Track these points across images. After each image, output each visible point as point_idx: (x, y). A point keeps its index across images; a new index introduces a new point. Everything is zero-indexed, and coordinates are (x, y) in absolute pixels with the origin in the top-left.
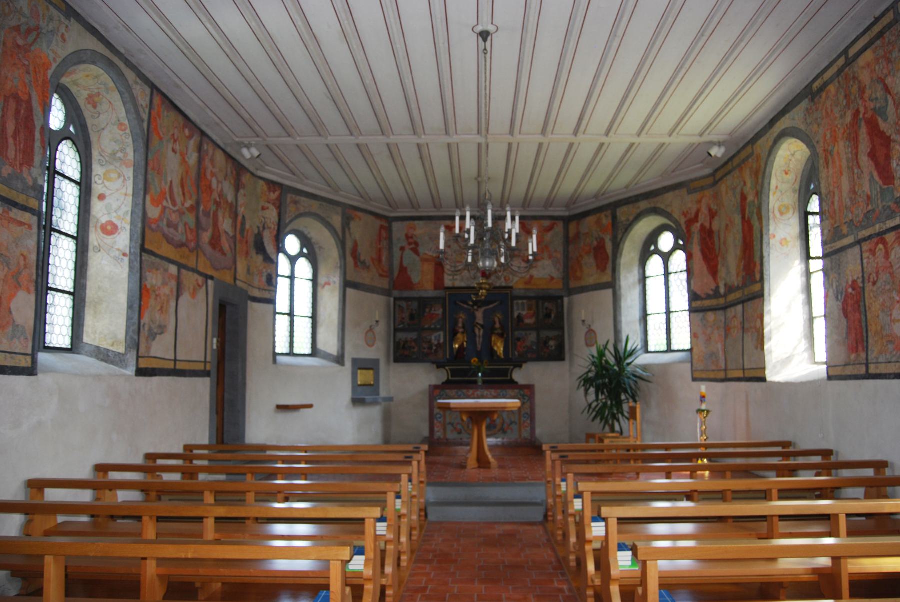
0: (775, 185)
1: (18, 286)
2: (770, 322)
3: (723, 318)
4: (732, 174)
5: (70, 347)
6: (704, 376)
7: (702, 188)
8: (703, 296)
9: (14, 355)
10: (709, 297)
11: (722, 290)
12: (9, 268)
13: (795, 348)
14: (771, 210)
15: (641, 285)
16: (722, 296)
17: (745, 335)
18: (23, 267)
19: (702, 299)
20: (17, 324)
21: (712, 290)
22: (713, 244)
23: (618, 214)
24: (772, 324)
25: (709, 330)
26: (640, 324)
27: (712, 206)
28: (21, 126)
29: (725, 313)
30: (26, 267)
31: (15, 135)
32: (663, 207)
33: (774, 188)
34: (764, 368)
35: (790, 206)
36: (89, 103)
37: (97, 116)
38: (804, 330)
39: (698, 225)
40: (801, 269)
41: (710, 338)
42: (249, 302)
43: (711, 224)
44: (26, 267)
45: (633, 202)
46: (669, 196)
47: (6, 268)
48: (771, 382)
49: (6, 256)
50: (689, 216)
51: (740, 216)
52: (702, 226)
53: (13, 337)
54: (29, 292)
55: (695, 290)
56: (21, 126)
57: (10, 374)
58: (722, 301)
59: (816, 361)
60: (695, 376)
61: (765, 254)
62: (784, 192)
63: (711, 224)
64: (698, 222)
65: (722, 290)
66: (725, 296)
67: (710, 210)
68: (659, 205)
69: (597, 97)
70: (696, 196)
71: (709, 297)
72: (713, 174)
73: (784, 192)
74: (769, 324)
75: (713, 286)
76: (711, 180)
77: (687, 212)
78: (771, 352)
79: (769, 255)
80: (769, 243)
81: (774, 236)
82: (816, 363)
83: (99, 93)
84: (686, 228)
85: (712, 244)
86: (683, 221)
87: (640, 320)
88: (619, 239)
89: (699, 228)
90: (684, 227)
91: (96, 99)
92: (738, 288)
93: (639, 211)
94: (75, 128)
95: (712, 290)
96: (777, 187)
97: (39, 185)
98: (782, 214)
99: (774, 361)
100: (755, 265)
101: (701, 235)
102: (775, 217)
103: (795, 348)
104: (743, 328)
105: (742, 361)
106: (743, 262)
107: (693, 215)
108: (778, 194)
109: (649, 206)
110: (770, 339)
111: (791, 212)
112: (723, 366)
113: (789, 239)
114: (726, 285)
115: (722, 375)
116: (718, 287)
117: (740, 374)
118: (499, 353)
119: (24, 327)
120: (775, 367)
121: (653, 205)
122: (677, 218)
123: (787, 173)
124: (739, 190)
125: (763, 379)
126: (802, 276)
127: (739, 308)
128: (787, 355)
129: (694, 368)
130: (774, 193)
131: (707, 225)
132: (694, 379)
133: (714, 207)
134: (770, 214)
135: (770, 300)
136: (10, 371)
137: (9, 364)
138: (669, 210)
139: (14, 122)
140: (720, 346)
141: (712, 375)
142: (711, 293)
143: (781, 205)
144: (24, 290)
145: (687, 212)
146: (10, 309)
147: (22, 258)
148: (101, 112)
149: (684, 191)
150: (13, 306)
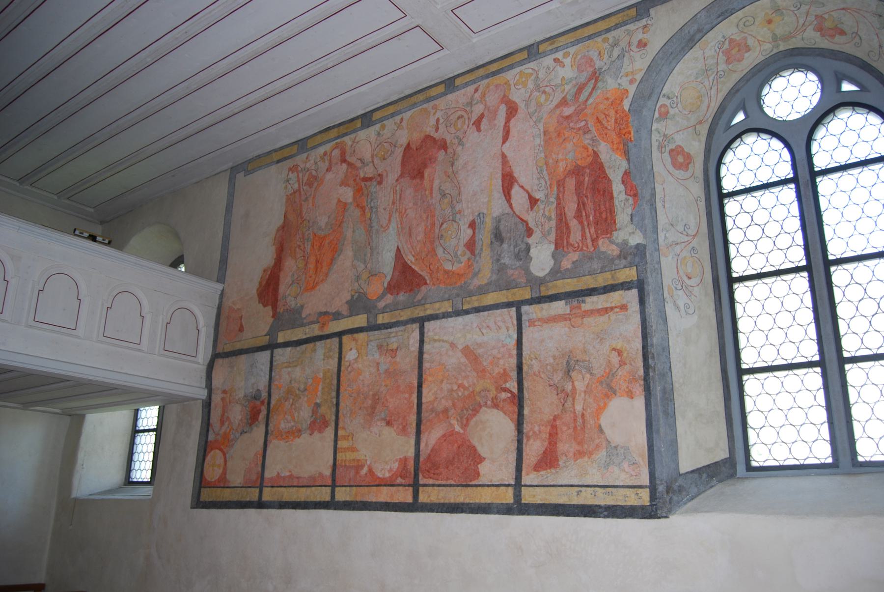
1: (611, 392)
5: (830, 460)
9: (614, 490)
12: (591, 374)
18: (617, 366)
20: (613, 445)
28: (586, 197)
30: (622, 363)
31: (578, 216)
36: (833, 36)
37: (857, 40)
42: (158, 407)
44: (622, 363)
47: (588, 376)
49: (584, 361)
53: (607, 466)
54: (631, 395)
56: (586, 197)
57: (605, 517)
69: (12, 28)
83: (817, 17)
91: (828, 24)
94: (852, 81)
97: (631, 247)
119: (627, 449)
136: (606, 513)
137: (602, 503)
139: (575, 199)
144: (622, 396)
146: (600, 426)
147: (615, 354)
148: (855, 30)
150: (604, 421)
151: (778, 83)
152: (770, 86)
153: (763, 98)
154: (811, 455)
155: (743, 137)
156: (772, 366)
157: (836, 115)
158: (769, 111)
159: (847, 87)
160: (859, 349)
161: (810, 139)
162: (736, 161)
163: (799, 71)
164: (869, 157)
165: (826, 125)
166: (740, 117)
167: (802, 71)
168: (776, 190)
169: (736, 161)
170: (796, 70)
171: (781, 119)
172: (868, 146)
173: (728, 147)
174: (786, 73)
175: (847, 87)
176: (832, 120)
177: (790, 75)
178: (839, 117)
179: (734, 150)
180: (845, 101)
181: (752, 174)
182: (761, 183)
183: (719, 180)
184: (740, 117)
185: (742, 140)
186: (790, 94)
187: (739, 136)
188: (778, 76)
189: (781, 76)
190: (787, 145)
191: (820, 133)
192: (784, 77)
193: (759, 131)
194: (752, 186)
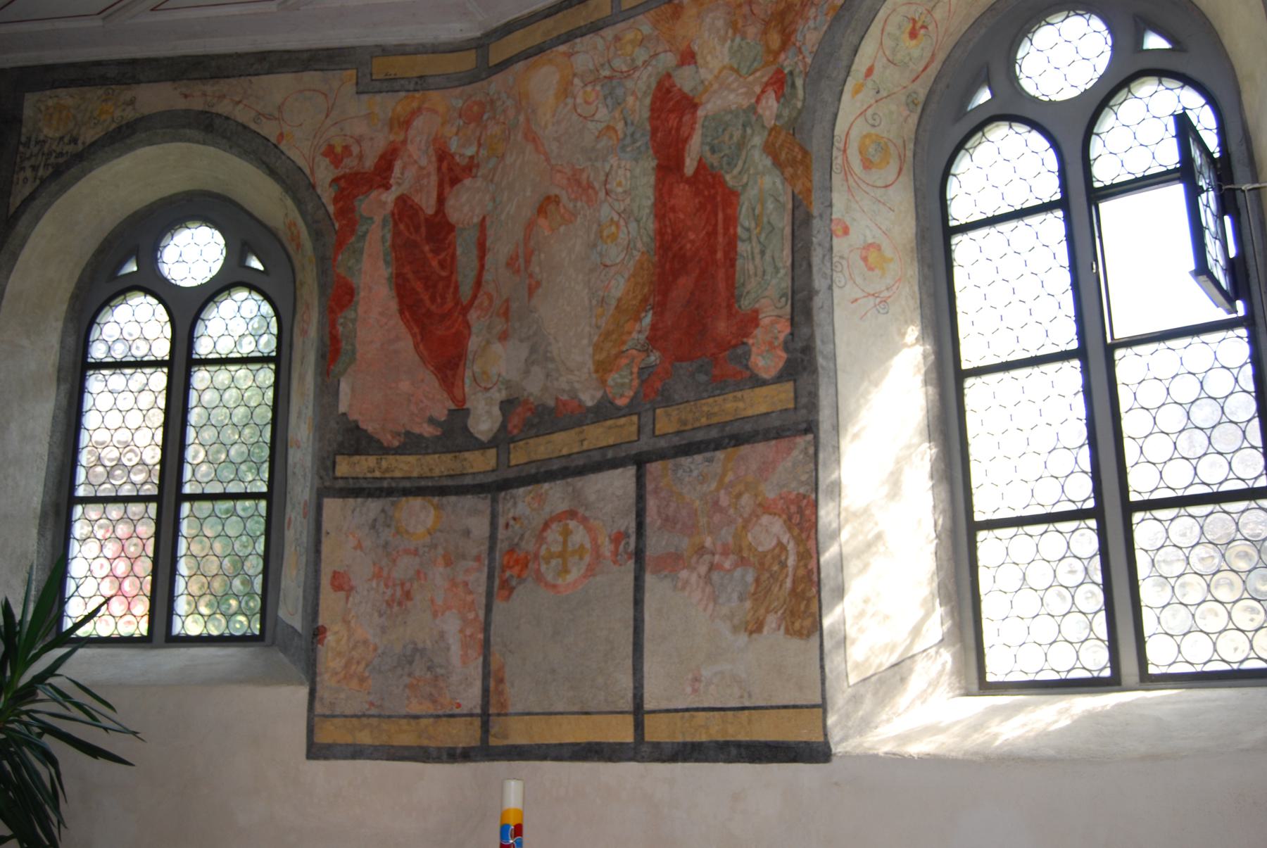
0: (868, 64)
2: (839, 529)
3: (480, 527)
4: (609, 33)
5: (1107, 673)
6: (365, 738)
7: (422, 83)
8: (387, 439)
10: (412, 444)
11: (484, 422)
13: (916, 631)
14: (838, 144)
15: (65, 387)
16: (482, 446)
17: (649, 579)
19: (384, 450)
21: (432, 421)
22: (450, 264)
23: (28, 112)
24: (845, 535)
25: (405, 567)
26: (41, 534)
27: (454, 146)
29: (494, 501)
32: (242, 115)
33: (864, 70)
34: (822, 707)
35: (892, 149)
38: (939, 568)
39: (389, 197)
40: (925, 357)
41: (408, 595)
43: (441, 200)
45: (104, 81)
46: (279, 86)
48: (846, 756)
50: (350, 164)
51: (650, 163)
52: (402, 200)
55: (354, 416)
58: (480, 463)
59: (990, 678)
60: (322, 738)
61: (819, 283)
62: (884, 93)
63: (441, 200)
64: (387, 187)
65: (484, 422)
66: (501, 440)
67: (443, 156)
68: (223, 108)
70: (387, 105)
71: (412, 444)
72: (480, 45)
73: (884, 93)
74: (836, 534)
75: (440, 408)
76: (468, 61)
77: (346, 148)
78: (843, 642)
79: (830, 288)
80: (831, 248)
81: (846, 231)
82: (987, 688)
84: (336, 200)
85: (442, 265)
86: (324, 174)
87: (44, 516)
88: (16, 201)
89: (390, 206)
90: (327, 194)
92: (604, 411)
93: (130, 115)
95: (432, 421)
96: (870, 71)
98: (867, 164)
99: (853, 679)
100: (752, 320)
101: (397, 234)
102: (847, 170)
103: (916, 631)
104: (639, 555)
105: (626, 682)
106: (648, 319)
107: (369, 163)
108: (867, 96)
109: (181, 104)
110: (840, 592)
111: (893, 166)
112: (471, 698)
113: (888, 251)
114: (507, 406)
115: (465, 734)
116: (460, 412)
117: (623, 732)
118: (11, 200)
120: (856, 699)
121: (197, 104)
122: (301, 163)
123: (913, 35)
124: (644, 81)
125: (818, 753)
126: (926, 383)
127: (620, 482)
128: (894, 659)
129: (319, 709)
130: (857, 91)
131: (427, 204)
132: (316, 751)
133: (462, 149)
134: (835, 153)
135: (837, 448)
138: (268, 130)
140: (451, 625)
141: (406, 738)
142: (428, 430)
143: (868, 136)
145: (346, 148)
149: (342, 81)
151: (1044, 35)
152: (1031, 40)
153: (1019, 61)
154: (1253, 655)
155: (1132, 85)
156: (1218, 493)
157: (1132, 90)
158: (1028, 86)
159: (1154, 42)
160: (1157, 488)
161: (1089, 133)
162: (1119, 130)
163: (1077, 14)
164: (1025, 206)
165: (1115, 108)
166: (984, 96)
167: (1082, 15)
168: (1005, 227)
169: (1119, 130)
170: (1072, 13)
171: (1046, 99)
172: (1146, 153)
173: (960, 146)
174: (1055, 19)
175: (1154, 42)
176: (1125, 100)
177: (1062, 21)
178: (1136, 95)
179: (1115, 108)
180: (972, 127)
181: (1146, 153)
182: (1012, 209)
183: (1087, 164)
184: (984, 96)
185: (984, 135)
186: (1063, 54)
187: (980, 127)
188: (1043, 23)
189: (1048, 24)
190: (1055, 145)
191: (1107, 122)
192: (1052, 24)
193: (1011, 118)
194: (1024, 206)
